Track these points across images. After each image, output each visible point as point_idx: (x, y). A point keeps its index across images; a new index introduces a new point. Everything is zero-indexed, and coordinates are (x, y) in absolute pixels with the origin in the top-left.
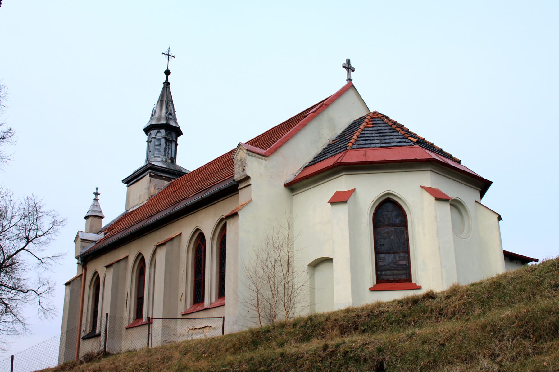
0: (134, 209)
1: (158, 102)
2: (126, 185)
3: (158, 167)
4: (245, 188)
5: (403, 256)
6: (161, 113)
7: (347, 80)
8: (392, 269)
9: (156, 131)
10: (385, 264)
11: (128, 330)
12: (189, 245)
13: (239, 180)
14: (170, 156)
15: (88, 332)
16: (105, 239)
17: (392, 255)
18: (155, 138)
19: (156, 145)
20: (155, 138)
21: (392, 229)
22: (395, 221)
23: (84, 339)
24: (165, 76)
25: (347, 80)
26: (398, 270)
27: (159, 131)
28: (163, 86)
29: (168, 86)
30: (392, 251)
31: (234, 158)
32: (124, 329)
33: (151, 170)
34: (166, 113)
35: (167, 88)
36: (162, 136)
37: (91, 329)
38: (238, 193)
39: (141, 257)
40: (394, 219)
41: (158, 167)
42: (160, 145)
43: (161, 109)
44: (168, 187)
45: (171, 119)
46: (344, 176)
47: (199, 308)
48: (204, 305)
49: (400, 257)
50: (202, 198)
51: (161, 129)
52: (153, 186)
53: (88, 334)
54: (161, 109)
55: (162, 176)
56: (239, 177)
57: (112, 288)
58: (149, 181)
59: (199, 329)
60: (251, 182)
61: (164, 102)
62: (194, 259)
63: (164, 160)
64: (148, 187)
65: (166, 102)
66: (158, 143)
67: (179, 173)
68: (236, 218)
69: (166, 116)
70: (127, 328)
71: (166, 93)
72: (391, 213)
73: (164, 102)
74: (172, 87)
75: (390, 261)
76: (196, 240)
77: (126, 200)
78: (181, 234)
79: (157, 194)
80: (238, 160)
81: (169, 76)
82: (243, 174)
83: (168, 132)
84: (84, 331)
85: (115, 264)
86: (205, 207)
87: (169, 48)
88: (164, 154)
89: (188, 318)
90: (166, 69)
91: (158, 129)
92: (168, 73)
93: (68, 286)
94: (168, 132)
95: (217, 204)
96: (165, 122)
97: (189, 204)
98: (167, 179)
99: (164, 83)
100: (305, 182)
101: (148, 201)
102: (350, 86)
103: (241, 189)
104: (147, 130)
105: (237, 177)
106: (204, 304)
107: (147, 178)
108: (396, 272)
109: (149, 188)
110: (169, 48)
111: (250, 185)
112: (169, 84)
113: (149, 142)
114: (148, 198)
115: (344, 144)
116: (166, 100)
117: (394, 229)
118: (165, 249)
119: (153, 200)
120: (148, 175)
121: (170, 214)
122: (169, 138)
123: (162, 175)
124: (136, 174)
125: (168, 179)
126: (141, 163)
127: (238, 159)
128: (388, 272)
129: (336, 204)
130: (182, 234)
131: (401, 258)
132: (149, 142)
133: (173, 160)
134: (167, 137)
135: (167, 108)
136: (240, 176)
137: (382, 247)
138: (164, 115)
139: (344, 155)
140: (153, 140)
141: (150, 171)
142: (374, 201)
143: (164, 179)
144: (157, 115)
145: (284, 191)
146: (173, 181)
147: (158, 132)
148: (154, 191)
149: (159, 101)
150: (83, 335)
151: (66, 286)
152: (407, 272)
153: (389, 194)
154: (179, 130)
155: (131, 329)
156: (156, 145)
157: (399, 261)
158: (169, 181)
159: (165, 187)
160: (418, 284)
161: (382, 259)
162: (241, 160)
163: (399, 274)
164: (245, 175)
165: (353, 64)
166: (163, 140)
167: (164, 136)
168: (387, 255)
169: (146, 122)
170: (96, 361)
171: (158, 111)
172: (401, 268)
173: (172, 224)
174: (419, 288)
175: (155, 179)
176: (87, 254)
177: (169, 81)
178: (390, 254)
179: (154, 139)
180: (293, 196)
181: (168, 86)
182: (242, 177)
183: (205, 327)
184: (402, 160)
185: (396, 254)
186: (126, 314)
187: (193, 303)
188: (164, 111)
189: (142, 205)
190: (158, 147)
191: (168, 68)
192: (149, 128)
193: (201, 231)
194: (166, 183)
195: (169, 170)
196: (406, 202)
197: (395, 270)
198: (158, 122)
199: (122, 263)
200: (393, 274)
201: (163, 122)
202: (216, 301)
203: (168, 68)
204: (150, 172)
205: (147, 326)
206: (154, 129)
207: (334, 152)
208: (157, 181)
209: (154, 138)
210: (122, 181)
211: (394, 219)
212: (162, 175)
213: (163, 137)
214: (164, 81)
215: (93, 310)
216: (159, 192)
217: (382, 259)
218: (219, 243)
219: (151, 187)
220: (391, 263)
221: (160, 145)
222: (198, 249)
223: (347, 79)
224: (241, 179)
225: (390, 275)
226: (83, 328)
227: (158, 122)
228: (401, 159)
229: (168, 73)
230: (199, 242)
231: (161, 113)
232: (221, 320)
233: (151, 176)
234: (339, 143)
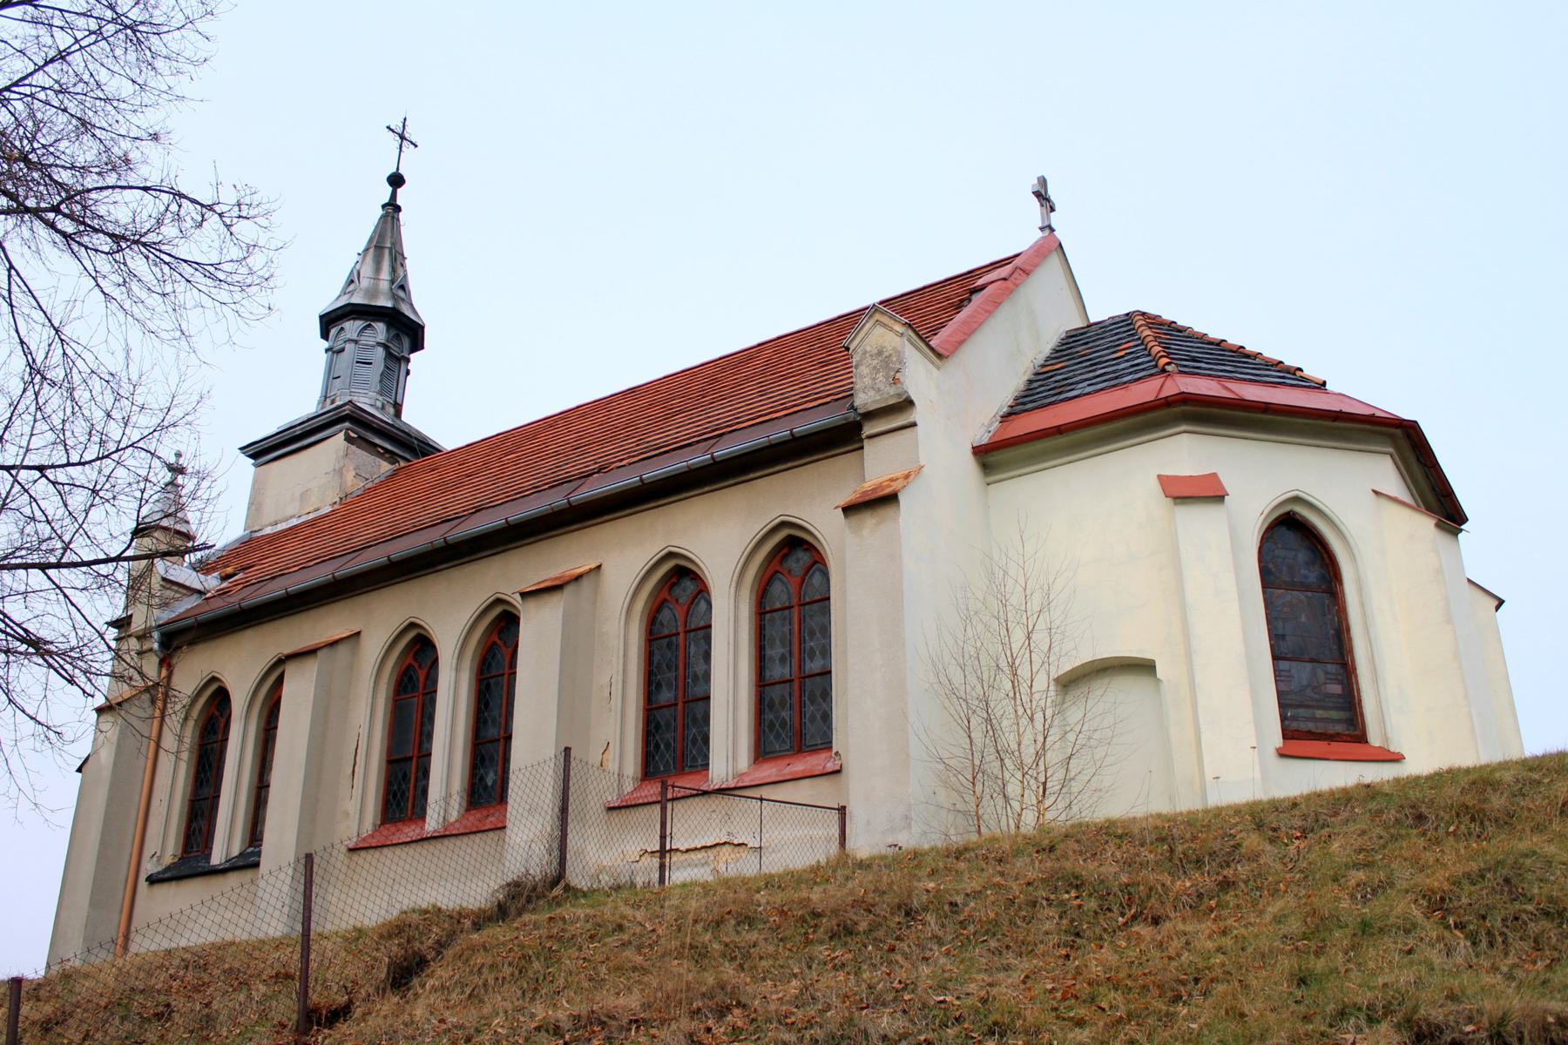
0: (281, 527)
1: (367, 250)
2: (253, 461)
3: (370, 418)
4: (888, 435)
5: (1334, 671)
6: (376, 279)
7: (1042, 229)
8: (1311, 703)
9: (359, 324)
10: (1292, 687)
11: (355, 857)
12: (462, 647)
13: (871, 408)
14: (393, 397)
15: (168, 860)
16: (222, 593)
17: (1309, 665)
18: (356, 342)
19: (358, 362)
20: (356, 342)
21: (1301, 596)
22: (1306, 577)
23: (153, 880)
24: (390, 189)
25: (1042, 229)
26: (1324, 708)
27: (369, 326)
28: (380, 212)
29: (396, 215)
30: (1306, 657)
31: (852, 348)
32: (340, 854)
33: (351, 423)
34: (392, 282)
35: (393, 217)
36: (378, 340)
37: (179, 853)
38: (862, 448)
39: (214, 687)
40: (1303, 571)
41: (370, 418)
42: (370, 363)
43: (378, 269)
44: (395, 473)
45: (403, 300)
46: (1185, 435)
47: (411, 832)
48: (422, 828)
49: (1327, 673)
50: (641, 480)
51: (373, 321)
52: (351, 468)
53: (168, 869)
54: (378, 269)
55: (376, 445)
56: (873, 402)
57: (312, 721)
58: (341, 453)
59: (687, 851)
60: (917, 415)
61: (387, 252)
62: (643, 643)
63: (379, 404)
64: (337, 468)
65: (391, 253)
66: (365, 356)
67: (415, 447)
68: (886, 512)
69: (391, 289)
70: (351, 850)
71: (393, 234)
72: (1294, 553)
73: (387, 252)
74: (407, 219)
75: (1305, 683)
76: (401, 653)
77: (251, 504)
78: (599, 567)
79: (360, 492)
80: (865, 352)
81: (399, 190)
82: (892, 391)
83: (393, 332)
84: (155, 859)
85: (325, 650)
86: (706, 489)
87: (405, 119)
88: (378, 388)
89: (761, 799)
90: (395, 170)
91: (367, 320)
92: (396, 181)
93: (108, 718)
94: (393, 332)
95: (759, 480)
96: (389, 304)
97: (577, 500)
98: (387, 456)
99: (384, 206)
100: (1039, 446)
101: (336, 507)
102: (1050, 247)
103: (871, 437)
104: (329, 322)
105: (865, 399)
106: (708, 775)
107: (336, 444)
108: (1319, 713)
109: (340, 472)
110: (405, 119)
111: (914, 425)
112: (398, 209)
113: (334, 352)
114: (338, 500)
115: (1129, 364)
116: (391, 249)
117: (1306, 597)
118: (562, 604)
119: (349, 507)
120: (342, 435)
121: (444, 544)
122: (395, 350)
123: (377, 441)
124: (298, 431)
125: (391, 457)
126: (304, 403)
127: (868, 349)
128: (1302, 712)
129: (1192, 503)
130: (362, 634)
131: (1328, 676)
132: (334, 352)
133: (398, 408)
134: (390, 345)
135: (393, 270)
136: (878, 398)
137: (1281, 643)
138: (384, 285)
139: (66, 675)
140: (349, 347)
141: (347, 424)
142: (1265, 513)
143: (381, 456)
144: (365, 283)
145: (969, 463)
146: (403, 464)
147: (365, 328)
148: (353, 484)
149: (372, 250)
150: (149, 867)
151: (98, 716)
152: (1295, 725)
153: (1297, 500)
154: (420, 333)
155: (648, 807)
156: (358, 362)
157: (1326, 683)
158: (393, 464)
159: (382, 478)
160: (1392, 749)
161: (1283, 673)
162: (880, 353)
163: (1327, 719)
164: (899, 395)
165: (1053, 193)
166: (380, 351)
167: (383, 341)
168: (1294, 664)
169: (329, 298)
170: (1211, 815)
171: (367, 270)
172: (1331, 705)
173: (558, 538)
174: (1395, 757)
175: (359, 451)
176: (192, 620)
177: (399, 203)
178: (1303, 664)
179: (353, 345)
180: (988, 484)
181: (396, 215)
182: (887, 399)
183: (739, 845)
184: (1341, 412)
185: (1315, 664)
186: (352, 806)
187: (640, 775)
188: (385, 275)
189: (311, 516)
190: (364, 369)
191: (398, 169)
192: (340, 312)
193: (422, 632)
194: (385, 467)
195: (403, 435)
196: (1342, 527)
197: (1318, 708)
198: (371, 299)
199: (342, 650)
200: (1314, 719)
201: (385, 302)
202: (749, 766)
203: (398, 169)
204: (347, 429)
205: (658, 807)
206: (354, 319)
207: (1105, 381)
208: (361, 456)
209: (353, 340)
210: (240, 449)
211: (1303, 571)
212: (377, 441)
213: (379, 344)
214: (386, 200)
215: (188, 797)
216: (367, 487)
217: (1283, 673)
218: (754, 597)
219: (348, 471)
220: (1307, 686)
221: (370, 363)
222: (406, 679)
223: (1040, 224)
224: (883, 405)
225: (1307, 719)
226: (152, 846)
227: (371, 299)
228: (1338, 409)
229: (396, 181)
230: (410, 660)
231: (376, 279)
232: (835, 816)
233: (348, 439)
234: (1086, 367)
